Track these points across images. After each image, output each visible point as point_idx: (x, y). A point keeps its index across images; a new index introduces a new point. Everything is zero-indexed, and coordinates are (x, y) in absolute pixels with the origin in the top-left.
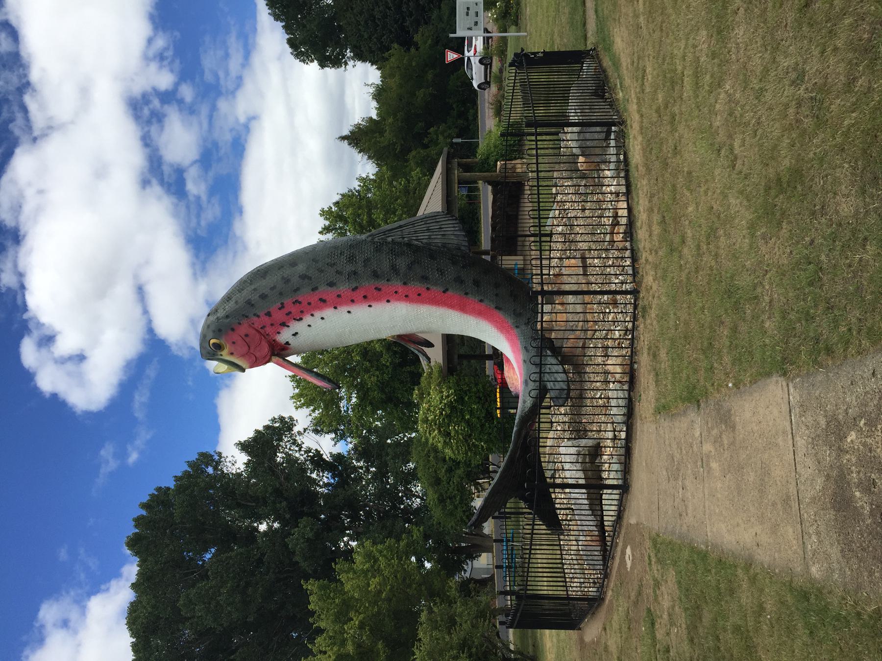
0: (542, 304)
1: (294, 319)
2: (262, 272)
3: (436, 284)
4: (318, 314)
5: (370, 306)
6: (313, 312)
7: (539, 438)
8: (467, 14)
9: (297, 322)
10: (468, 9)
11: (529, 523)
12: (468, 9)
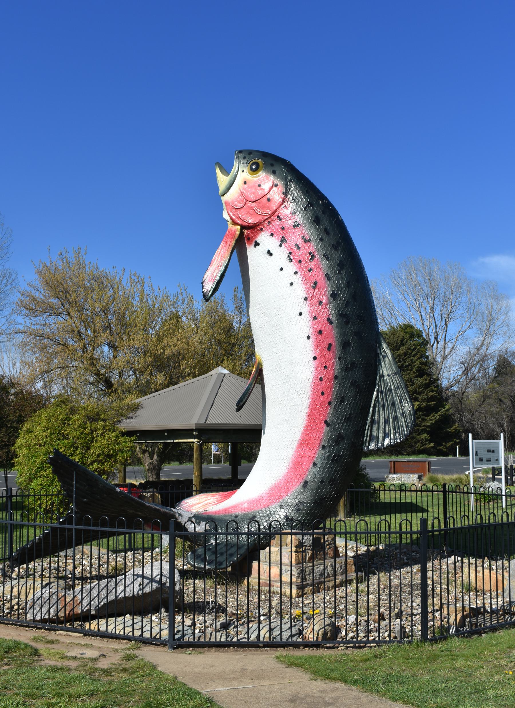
0: (313, 534)
1: (290, 253)
2: (223, 210)
3: (335, 413)
4: (298, 279)
5: (309, 337)
6: (299, 273)
7: (446, 530)
8: (489, 451)
9: (287, 255)
10: (493, 452)
11: (510, 518)
12: (493, 452)
